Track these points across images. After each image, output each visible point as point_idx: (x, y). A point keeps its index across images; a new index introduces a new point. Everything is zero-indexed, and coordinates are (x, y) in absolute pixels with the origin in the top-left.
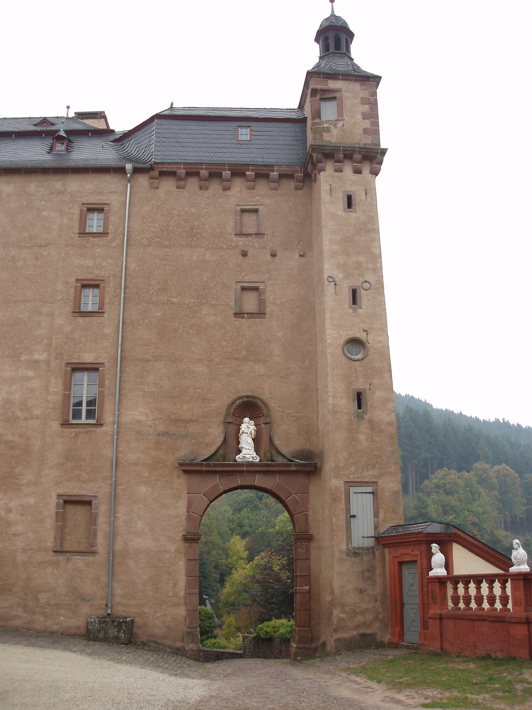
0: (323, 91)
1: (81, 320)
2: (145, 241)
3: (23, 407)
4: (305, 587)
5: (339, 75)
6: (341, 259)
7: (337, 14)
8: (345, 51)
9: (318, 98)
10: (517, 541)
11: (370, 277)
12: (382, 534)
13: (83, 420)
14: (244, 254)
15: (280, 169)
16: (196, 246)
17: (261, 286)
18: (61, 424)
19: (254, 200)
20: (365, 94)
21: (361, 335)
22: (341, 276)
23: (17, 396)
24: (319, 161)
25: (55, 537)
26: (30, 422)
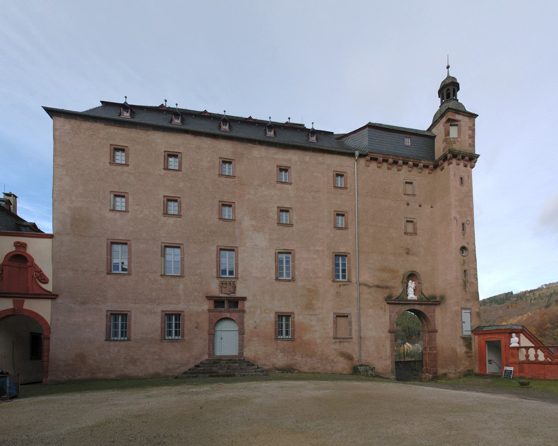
1: (338, 231)
3: (313, 272)
4: (435, 352)
9: (449, 124)
11: (469, 218)
13: (341, 279)
14: (408, 205)
15: (424, 162)
17: (415, 220)
18: (332, 281)
19: (411, 177)
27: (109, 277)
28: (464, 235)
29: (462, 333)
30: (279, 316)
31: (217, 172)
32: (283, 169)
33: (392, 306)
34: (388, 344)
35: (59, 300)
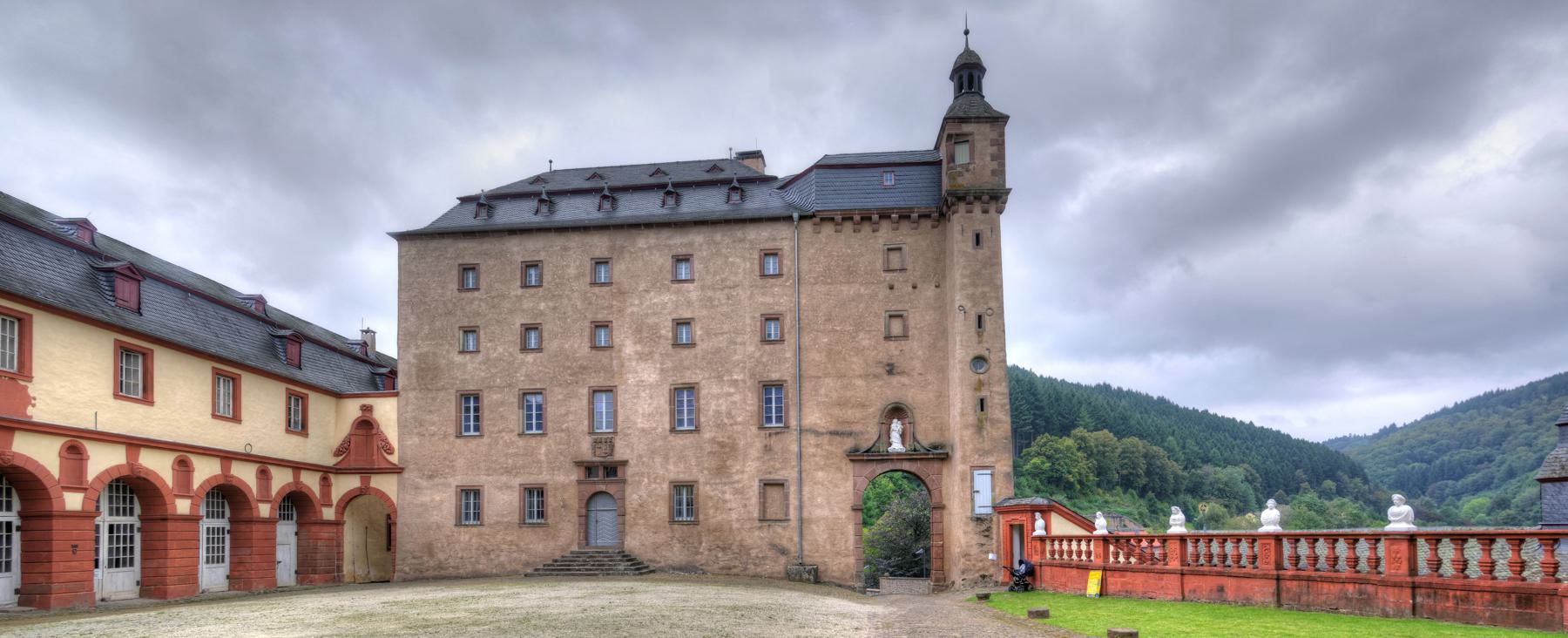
0: (957, 135)
1: (767, 347)
2: (812, 280)
5: (971, 118)
6: (970, 291)
7: (972, 47)
8: (977, 90)
10: (1099, 513)
11: (993, 304)
12: (999, 504)
14: (891, 288)
16: (853, 282)
17: (905, 314)
20: (994, 135)
21: (986, 353)
22: (969, 305)
23: (723, 408)
24: (953, 204)
25: (759, 510)
26: (735, 427)
27: (459, 441)
29: (973, 509)
30: (675, 486)
31: (588, 280)
32: (681, 259)
33: (858, 466)
34: (850, 529)
35: (406, 475)
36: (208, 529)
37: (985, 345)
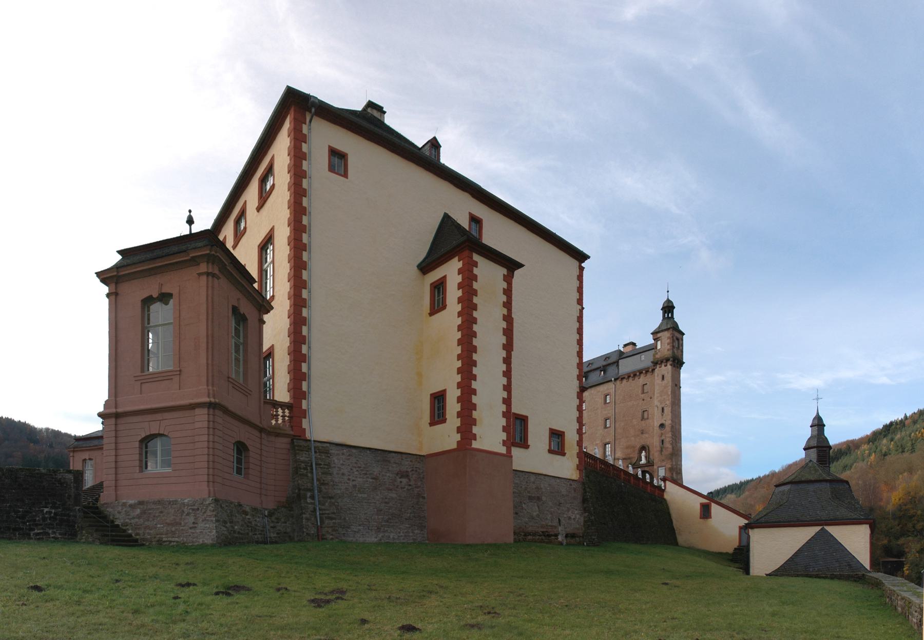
7: (670, 299)
17: (647, 409)
28: (662, 415)
36: (159, 283)
37: (664, 419)
